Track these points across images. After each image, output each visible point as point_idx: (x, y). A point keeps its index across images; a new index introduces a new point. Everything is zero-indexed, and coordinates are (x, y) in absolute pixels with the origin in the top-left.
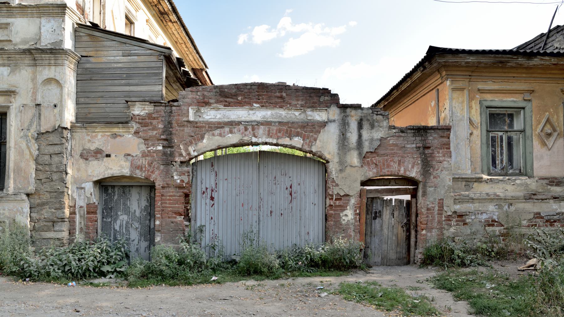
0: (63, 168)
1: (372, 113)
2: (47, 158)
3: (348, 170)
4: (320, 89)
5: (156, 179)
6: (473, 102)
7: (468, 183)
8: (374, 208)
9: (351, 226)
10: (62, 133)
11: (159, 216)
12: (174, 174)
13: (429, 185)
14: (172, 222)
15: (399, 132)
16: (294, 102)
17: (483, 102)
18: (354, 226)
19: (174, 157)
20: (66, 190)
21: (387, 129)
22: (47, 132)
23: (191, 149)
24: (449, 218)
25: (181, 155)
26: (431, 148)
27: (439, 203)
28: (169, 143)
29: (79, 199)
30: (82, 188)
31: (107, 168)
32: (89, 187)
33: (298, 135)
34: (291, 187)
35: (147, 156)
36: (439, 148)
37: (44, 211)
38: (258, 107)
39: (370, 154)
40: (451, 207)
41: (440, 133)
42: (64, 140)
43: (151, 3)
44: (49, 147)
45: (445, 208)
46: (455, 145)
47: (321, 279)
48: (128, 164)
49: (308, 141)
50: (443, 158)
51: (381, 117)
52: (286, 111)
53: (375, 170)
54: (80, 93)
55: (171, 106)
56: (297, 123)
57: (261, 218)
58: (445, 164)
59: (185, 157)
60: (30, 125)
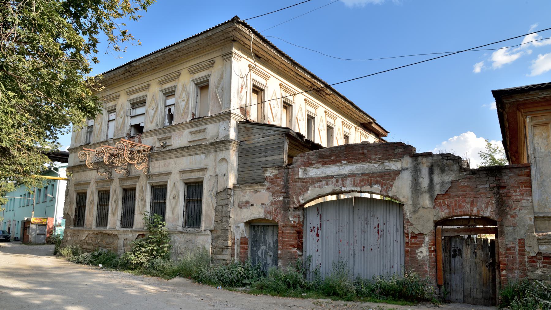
0: (227, 214)
1: (442, 159)
2: (220, 207)
3: (421, 211)
4: (394, 143)
5: (279, 220)
8: (453, 246)
9: (426, 262)
10: (228, 192)
11: (280, 247)
12: (290, 217)
13: (506, 224)
14: (289, 252)
15: (471, 173)
16: (373, 157)
18: (430, 262)
19: (290, 205)
20: (229, 228)
22: (221, 191)
23: (300, 198)
24: (533, 260)
25: (294, 203)
26: (507, 187)
27: (519, 243)
28: (287, 195)
29: (237, 234)
30: (239, 227)
31: (252, 214)
32: (242, 225)
33: (377, 183)
34: (378, 227)
35: (274, 204)
36: (516, 187)
37: (218, 242)
39: (441, 196)
40: (532, 249)
41: (517, 172)
42: (229, 196)
43: (307, 87)
44: (222, 201)
45: (527, 249)
46: (539, 183)
47: (385, 305)
48: (263, 210)
49: (385, 187)
50: (521, 197)
51: (451, 162)
52: (368, 164)
53: (447, 211)
54: (240, 165)
55: (289, 168)
56: (376, 173)
57: (356, 252)
58: (524, 203)
59: (296, 204)
60: (213, 188)
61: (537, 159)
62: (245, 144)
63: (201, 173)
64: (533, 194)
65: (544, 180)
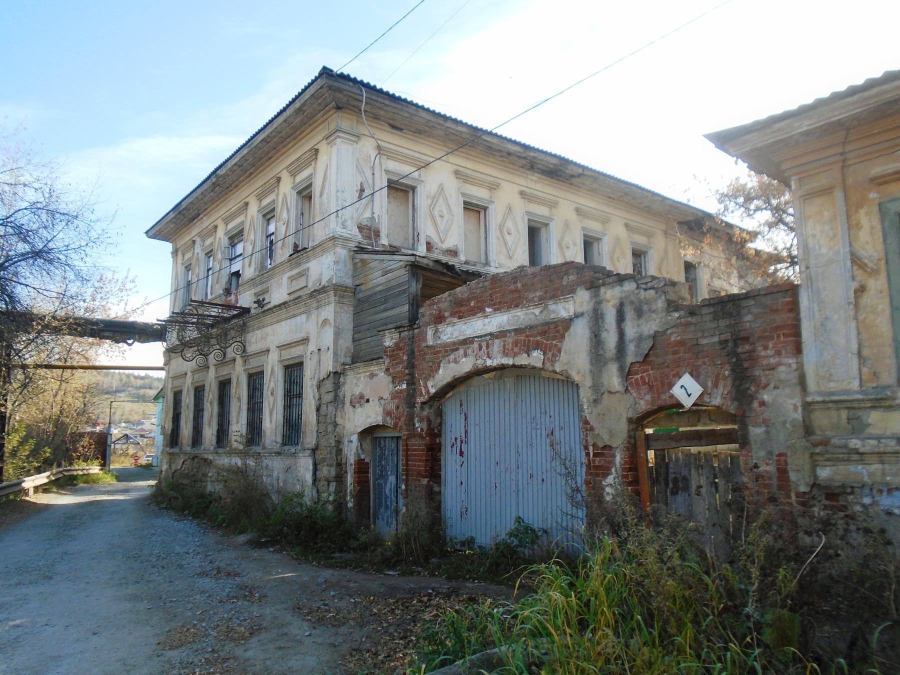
1: (638, 288)
3: (607, 400)
6: (862, 212)
7: (855, 412)
8: (671, 470)
17: (889, 205)
21: (664, 314)
25: (421, 394)
28: (412, 382)
33: (538, 346)
38: (490, 312)
39: (638, 365)
49: (550, 355)
50: (777, 359)
52: (525, 311)
53: (648, 397)
56: (536, 326)
61: (813, 270)
62: (361, 291)
63: (301, 347)
64: (805, 350)
65: (827, 318)
